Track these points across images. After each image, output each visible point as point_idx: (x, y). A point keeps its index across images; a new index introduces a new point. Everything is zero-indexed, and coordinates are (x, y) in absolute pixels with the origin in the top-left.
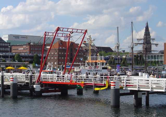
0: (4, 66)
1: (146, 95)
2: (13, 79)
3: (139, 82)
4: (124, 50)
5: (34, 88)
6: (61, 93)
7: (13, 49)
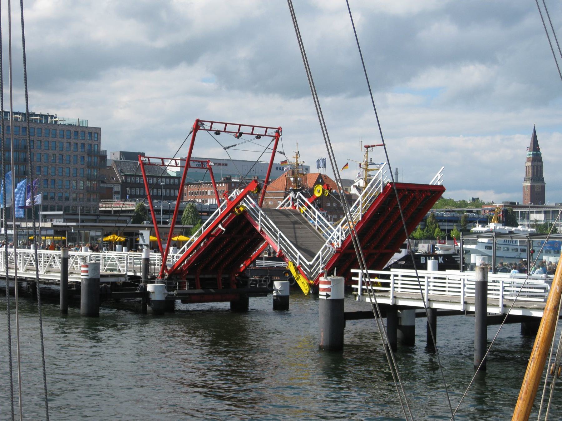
0: (99, 233)
1: (425, 320)
2: (87, 266)
3: (506, 289)
4: (475, 197)
5: (149, 293)
6: (232, 305)
7: (190, 193)
